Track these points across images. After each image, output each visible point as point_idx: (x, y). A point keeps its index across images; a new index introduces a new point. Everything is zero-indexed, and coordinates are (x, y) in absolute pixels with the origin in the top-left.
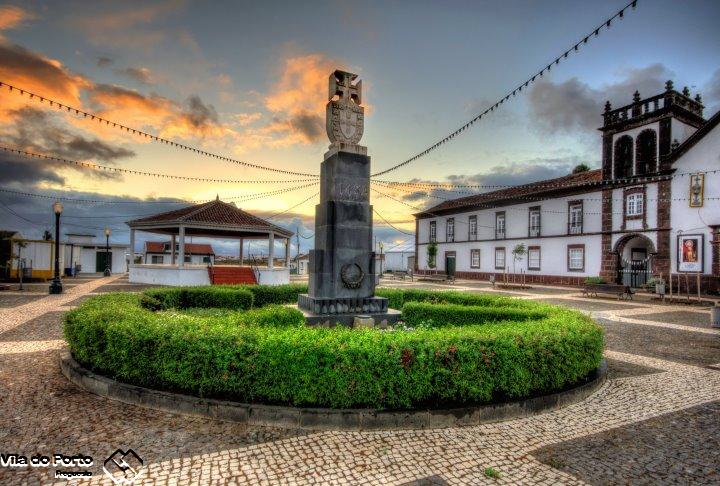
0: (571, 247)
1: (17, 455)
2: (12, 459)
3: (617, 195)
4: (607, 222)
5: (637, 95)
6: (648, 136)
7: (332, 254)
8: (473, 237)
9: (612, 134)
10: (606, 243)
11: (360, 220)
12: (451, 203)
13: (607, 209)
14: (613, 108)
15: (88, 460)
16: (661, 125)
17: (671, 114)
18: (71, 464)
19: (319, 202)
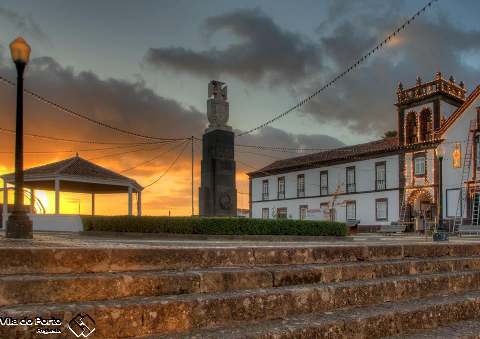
0: (378, 201)
1: (11, 318)
2: (8, 320)
3: (409, 156)
4: (402, 180)
5: (419, 81)
6: (426, 113)
7: (214, 189)
8: (301, 195)
9: (404, 110)
10: (402, 196)
11: (229, 170)
12: (282, 163)
13: (402, 169)
14: (405, 89)
15: (59, 321)
16: (434, 105)
17: (440, 97)
18: (47, 324)
19: (202, 160)
